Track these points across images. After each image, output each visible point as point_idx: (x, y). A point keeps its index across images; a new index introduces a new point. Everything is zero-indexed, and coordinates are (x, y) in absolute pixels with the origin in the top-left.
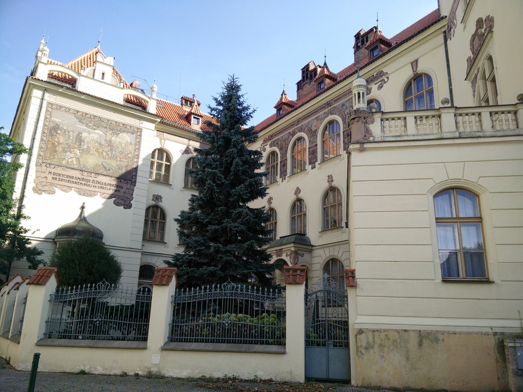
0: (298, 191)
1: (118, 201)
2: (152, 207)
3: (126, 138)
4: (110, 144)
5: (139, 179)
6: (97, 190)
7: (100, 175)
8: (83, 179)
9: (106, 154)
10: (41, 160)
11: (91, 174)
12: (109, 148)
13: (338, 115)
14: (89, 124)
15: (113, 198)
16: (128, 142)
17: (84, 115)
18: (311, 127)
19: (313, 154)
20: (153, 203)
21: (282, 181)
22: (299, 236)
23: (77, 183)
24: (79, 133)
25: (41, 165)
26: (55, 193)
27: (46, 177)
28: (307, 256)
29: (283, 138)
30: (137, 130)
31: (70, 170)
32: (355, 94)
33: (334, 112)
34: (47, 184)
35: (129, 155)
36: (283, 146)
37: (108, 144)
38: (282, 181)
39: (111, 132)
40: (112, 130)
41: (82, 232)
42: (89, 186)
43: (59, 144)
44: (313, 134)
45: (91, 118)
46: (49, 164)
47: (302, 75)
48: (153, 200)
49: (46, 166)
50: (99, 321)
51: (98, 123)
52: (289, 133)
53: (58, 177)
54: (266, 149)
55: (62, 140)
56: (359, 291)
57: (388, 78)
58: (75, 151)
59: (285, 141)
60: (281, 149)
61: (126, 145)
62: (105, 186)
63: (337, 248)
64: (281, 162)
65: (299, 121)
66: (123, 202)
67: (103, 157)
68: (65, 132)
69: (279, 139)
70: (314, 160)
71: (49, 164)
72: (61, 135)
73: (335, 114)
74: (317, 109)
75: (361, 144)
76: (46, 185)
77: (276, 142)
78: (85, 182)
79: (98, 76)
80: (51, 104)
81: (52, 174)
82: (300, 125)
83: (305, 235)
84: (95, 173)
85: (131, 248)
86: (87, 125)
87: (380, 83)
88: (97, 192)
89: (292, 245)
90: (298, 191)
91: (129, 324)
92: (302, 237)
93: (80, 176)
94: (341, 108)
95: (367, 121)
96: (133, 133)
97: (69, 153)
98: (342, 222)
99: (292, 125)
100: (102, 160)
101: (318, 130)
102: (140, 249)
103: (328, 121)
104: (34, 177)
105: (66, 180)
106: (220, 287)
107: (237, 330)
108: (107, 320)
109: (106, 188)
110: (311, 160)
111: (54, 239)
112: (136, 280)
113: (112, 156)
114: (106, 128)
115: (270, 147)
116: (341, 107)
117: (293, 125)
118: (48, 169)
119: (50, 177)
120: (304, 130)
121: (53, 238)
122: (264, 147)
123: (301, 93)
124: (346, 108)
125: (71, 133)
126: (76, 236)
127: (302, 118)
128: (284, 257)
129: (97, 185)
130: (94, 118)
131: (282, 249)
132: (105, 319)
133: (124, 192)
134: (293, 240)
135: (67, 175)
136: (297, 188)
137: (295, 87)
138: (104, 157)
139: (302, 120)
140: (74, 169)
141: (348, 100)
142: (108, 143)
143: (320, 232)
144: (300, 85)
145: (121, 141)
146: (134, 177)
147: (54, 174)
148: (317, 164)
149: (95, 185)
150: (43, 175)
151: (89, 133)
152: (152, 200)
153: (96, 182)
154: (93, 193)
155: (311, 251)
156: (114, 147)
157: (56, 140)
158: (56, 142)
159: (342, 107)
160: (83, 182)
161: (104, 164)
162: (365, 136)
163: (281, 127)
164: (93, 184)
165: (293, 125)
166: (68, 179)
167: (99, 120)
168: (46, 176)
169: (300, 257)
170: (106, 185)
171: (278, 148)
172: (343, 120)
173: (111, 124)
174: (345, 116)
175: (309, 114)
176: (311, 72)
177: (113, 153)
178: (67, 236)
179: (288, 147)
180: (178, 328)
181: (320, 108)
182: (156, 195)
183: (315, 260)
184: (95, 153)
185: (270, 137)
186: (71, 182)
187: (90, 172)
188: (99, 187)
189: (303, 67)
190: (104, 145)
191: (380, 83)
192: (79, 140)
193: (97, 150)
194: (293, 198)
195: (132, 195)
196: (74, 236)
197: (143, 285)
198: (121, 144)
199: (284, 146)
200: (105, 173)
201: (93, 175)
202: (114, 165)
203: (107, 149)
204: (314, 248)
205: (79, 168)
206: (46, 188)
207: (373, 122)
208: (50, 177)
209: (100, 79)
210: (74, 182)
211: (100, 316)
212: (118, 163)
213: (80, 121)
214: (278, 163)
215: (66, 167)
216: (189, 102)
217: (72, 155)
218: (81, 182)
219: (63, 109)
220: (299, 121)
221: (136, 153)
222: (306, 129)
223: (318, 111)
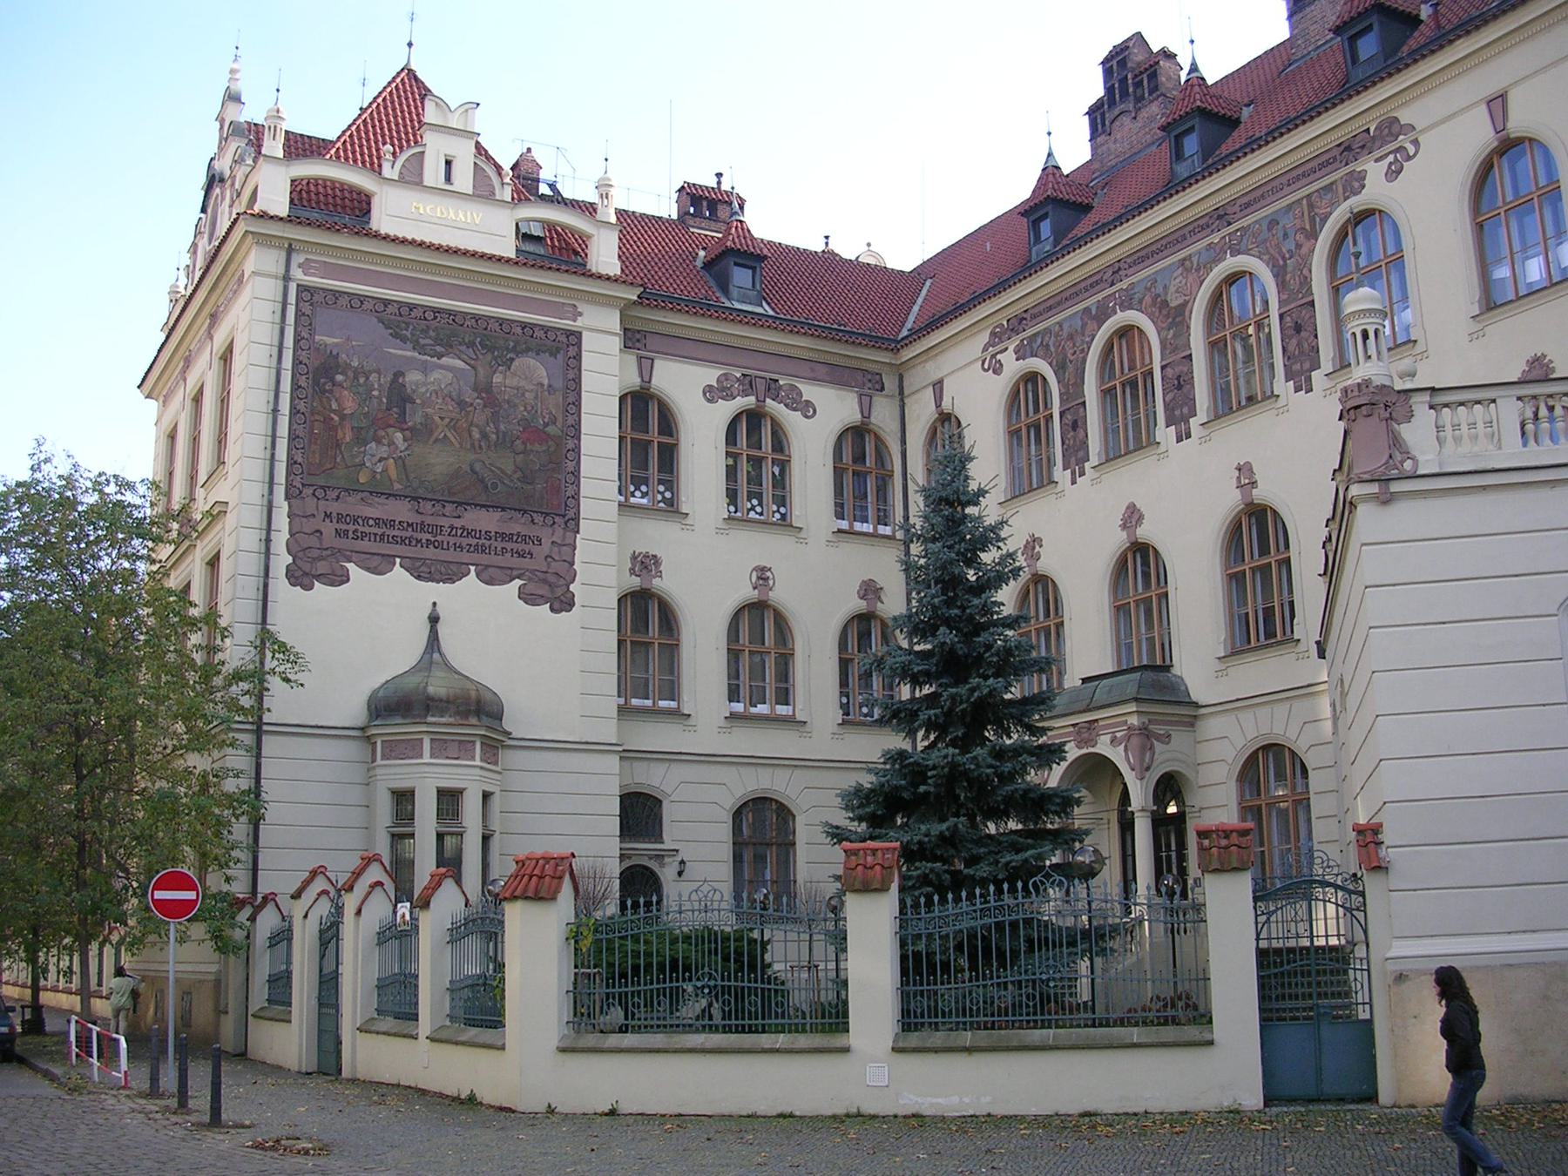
0: (1132, 516)
1: (531, 588)
2: (632, 597)
3: (535, 370)
4: (485, 391)
5: (586, 507)
6: (464, 557)
7: (468, 508)
8: (422, 527)
9: (481, 432)
10: (298, 478)
11: (444, 506)
12: (488, 411)
13: (1259, 258)
14: (422, 341)
15: (514, 579)
16: (542, 385)
17: (405, 311)
18: (1166, 294)
19: (1180, 387)
20: (635, 582)
21: (1074, 482)
22: (1150, 675)
23: (407, 542)
24: (399, 374)
25: (301, 492)
26: (348, 580)
27: (318, 531)
28: (1179, 738)
29: (1065, 326)
30: (565, 340)
31: (382, 500)
32: (1354, 334)
33: (1243, 247)
34: (325, 553)
35: (551, 429)
36: (1066, 356)
37: (482, 399)
38: (1074, 482)
39: (489, 356)
40: (491, 349)
41: (448, 702)
42: (438, 545)
43: (343, 417)
44: (1174, 319)
45: (425, 319)
46: (322, 487)
47: (1105, 82)
48: (632, 571)
49: (314, 494)
50: (709, 986)
51: (448, 332)
52: (1087, 310)
53: (351, 527)
54: (1001, 365)
55: (350, 406)
56: (1394, 880)
57: (1416, 142)
58: (390, 434)
59: (1071, 337)
60: (1059, 369)
61: (536, 398)
62: (487, 543)
63: (1281, 710)
64: (1062, 414)
65: (1120, 269)
66: (544, 591)
67: (473, 445)
68: (356, 378)
69: (1047, 331)
70: (1185, 410)
71: (322, 487)
72: (346, 389)
73: (1247, 252)
74: (1181, 233)
75: (1382, 483)
76: (321, 558)
77: (1039, 341)
78: (429, 536)
79: (433, 173)
80: (309, 291)
81: (335, 520)
82: (1124, 285)
83: (1167, 668)
84: (454, 502)
85: (587, 743)
86: (417, 347)
87: (1391, 158)
88: (467, 564)
89: (1132, 707)
90: (1132, 516)
91: (620, 994)
92: (1162, 676)
93: (413, 518)
94: (1265, 234)
95: (1394, 415)
96: (553, 354)
97: (373, 445)
98: (1295, 621)
99: (1093, 283)
100: (471, 457)
101: (1190, 304)
102: (614, 742)
103: (1223, 276)
104: (285, 535)
105: (375, 535)
106: (1025, 888)
107: (773, 1005)
108: (921, 988)
109: (493, 548)
110: (1173, 410)
111: (362, 729)
112: (613, 846)
113: (498, 438)
114: (471, 345)
115: (1017, 360)
116: (1265, 227)
117: (1097, 283)
118: (322, 503)
119: (329, 528)
120: (1140, 302)
121: (360, 722)
122: (994, 356)
123: (1104, 148)
124: (1286, 236)
125: (374, 377)
126: (432, 716)
127: (1129, 260)
128: (1103, 747)
129: (465, 542)
130: (435, 318)
131: (1096, 720)
132: (723, 980)
133: (546, 557)
134: (1131, 691)
135: (375, 516)
136: (1128, 508)
137: (1084, 124)
138: (476, 443)
139: (1130, 267)
140: (395, 496)
141: (1290, 207)
142: (484, 395)
143: (1219, 658)
144: (1099, 117)
145: (523, 383)
146: (571, 502)
147: (340, 518)
148: (1194, 422)
149: (459, 540)
150: (309, 526)
151: (425, 369)
152: (631, 574)
153: (459, 532)
154: (454, 568)
155: (1191, 722)
156: (501, 407)
157: (334, 406)
158: (335, 412)
159: (1269, 229)
160: (425, 537)
161: (478, 467)
162: (1391, 457)
163: (1055, 288)
164: (452, 540)
165: (1097, 283)
166: (380, 531)
167: (451, 322)
168: (317, 528)
169: (1158, 746)
170: (491, 539)
171: (1050, 364)
172: (1276, 276)
173: (486, 329)
174: (1281, 262)
175: (1154, 248)
176: (1136, 76)
177: (502, 427)
178: (404, 717)
179: (1084, 361)
180: (614, 998)
181: (1190, 228)
182: (640, 554)
183: (1209, 752)
184: (449, 434)
185: (1014, 321)
186: (390, 539)
187: (438, 501)
188: (472, 549)
189: (1105, 53)
190: (472, 404)
191: (1391, 158)
192: (400, 398)
193: (453, 425)
194: (1117, 540)
195: (572, 564)
196: (426, 717)
197: (630, 858)
198: (523, 395)
199: (1072, 358)
200: (482, 500)
201: (449, 508)
202: (509, 469)
203: (480, 417)
204: (1203, 711)
205: (408, 492)
206: (322, 567)
207: (1409, 416)
208: (329, 528)
209: (441, 184)
210: (399, 540)
211: (710, 974)
212: (520, 458)
213: (396, 336)
214: (1051, 416)
215: (371, 493)
216: (705, 203)
217: (383, 451)
218: (419, 536)
219: (344, 301)
220: (1117, 270)
221: (570, 421)
222: (1148, 299)
223: (1184, 238)
